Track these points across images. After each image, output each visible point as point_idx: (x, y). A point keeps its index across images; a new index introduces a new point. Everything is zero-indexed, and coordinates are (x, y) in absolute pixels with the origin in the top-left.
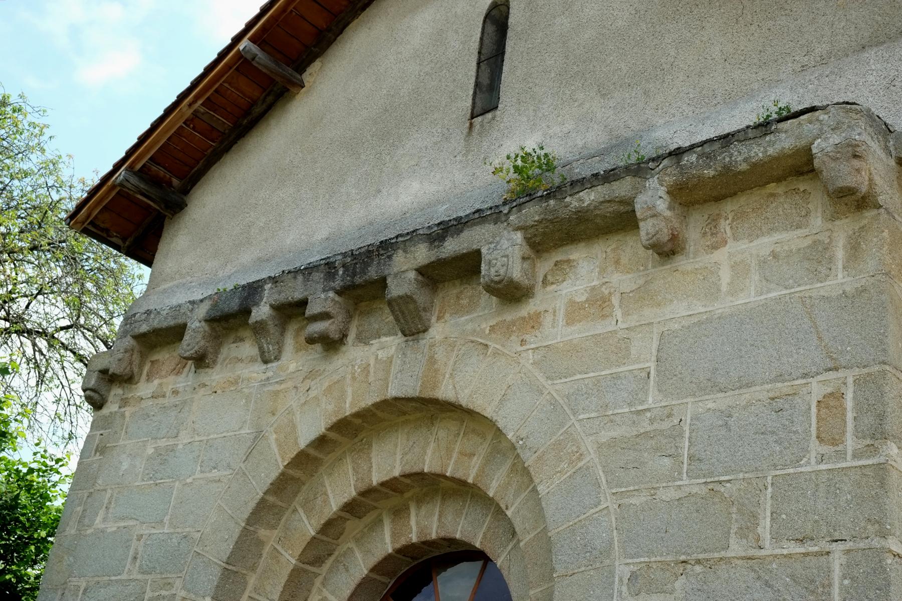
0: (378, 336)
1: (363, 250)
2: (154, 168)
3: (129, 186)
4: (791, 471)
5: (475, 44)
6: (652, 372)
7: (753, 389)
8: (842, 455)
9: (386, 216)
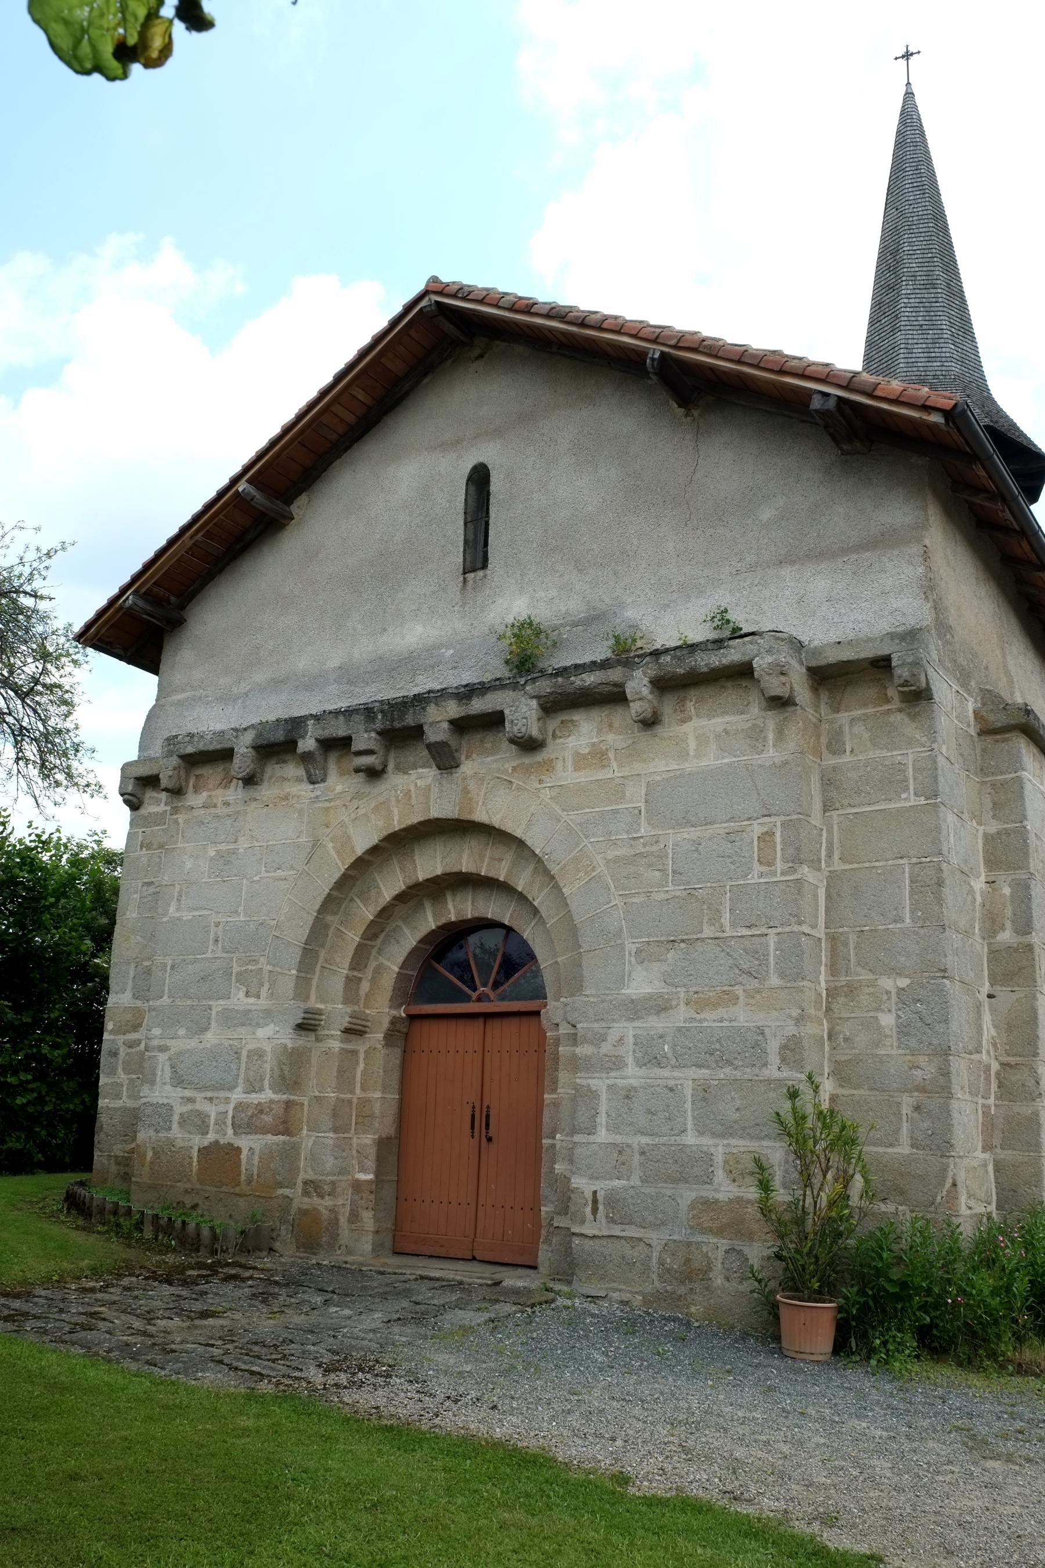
0: (415, 767)
1: (399, 700)
2: (155, 589)
3: (137, 608)
4: (742, 882)
5: (461, 506)
6: (643, 810)
7: (715, 826)
8: (774, 873)
9: (394, 653)
